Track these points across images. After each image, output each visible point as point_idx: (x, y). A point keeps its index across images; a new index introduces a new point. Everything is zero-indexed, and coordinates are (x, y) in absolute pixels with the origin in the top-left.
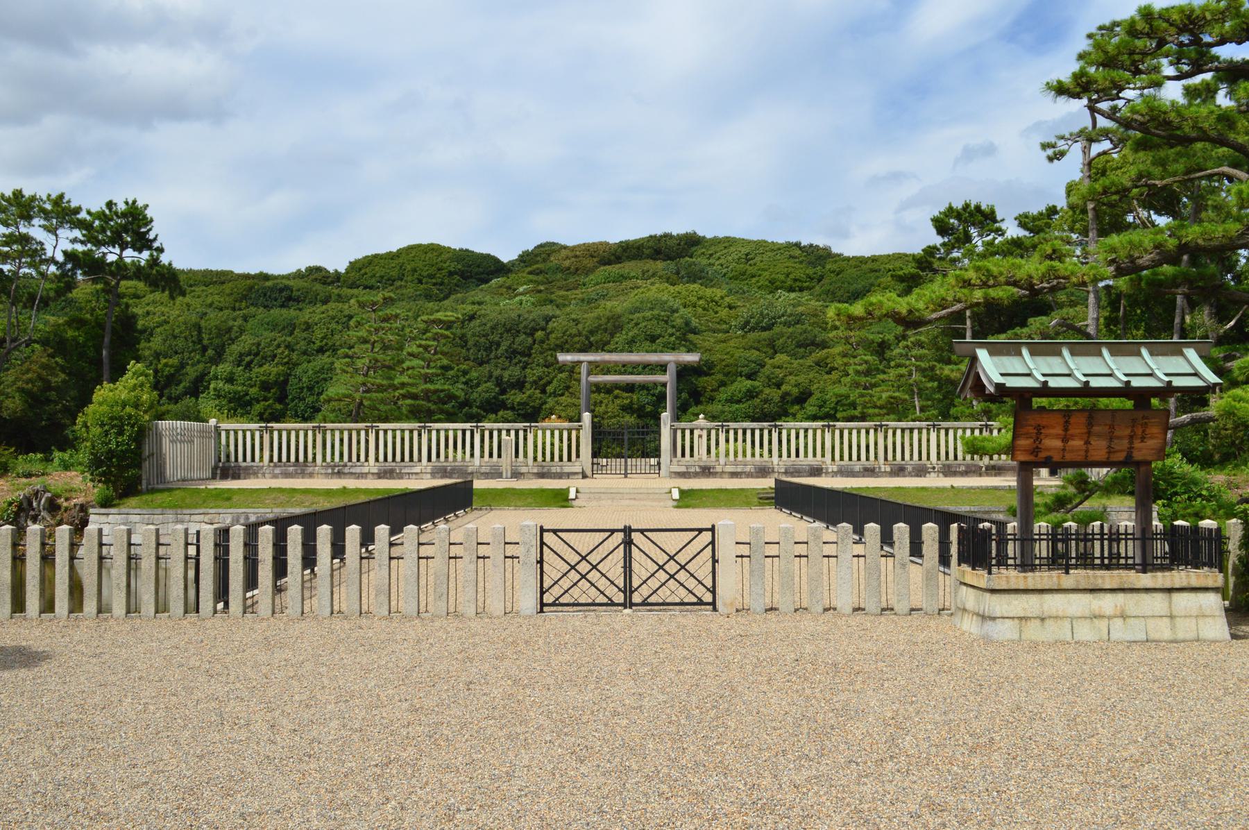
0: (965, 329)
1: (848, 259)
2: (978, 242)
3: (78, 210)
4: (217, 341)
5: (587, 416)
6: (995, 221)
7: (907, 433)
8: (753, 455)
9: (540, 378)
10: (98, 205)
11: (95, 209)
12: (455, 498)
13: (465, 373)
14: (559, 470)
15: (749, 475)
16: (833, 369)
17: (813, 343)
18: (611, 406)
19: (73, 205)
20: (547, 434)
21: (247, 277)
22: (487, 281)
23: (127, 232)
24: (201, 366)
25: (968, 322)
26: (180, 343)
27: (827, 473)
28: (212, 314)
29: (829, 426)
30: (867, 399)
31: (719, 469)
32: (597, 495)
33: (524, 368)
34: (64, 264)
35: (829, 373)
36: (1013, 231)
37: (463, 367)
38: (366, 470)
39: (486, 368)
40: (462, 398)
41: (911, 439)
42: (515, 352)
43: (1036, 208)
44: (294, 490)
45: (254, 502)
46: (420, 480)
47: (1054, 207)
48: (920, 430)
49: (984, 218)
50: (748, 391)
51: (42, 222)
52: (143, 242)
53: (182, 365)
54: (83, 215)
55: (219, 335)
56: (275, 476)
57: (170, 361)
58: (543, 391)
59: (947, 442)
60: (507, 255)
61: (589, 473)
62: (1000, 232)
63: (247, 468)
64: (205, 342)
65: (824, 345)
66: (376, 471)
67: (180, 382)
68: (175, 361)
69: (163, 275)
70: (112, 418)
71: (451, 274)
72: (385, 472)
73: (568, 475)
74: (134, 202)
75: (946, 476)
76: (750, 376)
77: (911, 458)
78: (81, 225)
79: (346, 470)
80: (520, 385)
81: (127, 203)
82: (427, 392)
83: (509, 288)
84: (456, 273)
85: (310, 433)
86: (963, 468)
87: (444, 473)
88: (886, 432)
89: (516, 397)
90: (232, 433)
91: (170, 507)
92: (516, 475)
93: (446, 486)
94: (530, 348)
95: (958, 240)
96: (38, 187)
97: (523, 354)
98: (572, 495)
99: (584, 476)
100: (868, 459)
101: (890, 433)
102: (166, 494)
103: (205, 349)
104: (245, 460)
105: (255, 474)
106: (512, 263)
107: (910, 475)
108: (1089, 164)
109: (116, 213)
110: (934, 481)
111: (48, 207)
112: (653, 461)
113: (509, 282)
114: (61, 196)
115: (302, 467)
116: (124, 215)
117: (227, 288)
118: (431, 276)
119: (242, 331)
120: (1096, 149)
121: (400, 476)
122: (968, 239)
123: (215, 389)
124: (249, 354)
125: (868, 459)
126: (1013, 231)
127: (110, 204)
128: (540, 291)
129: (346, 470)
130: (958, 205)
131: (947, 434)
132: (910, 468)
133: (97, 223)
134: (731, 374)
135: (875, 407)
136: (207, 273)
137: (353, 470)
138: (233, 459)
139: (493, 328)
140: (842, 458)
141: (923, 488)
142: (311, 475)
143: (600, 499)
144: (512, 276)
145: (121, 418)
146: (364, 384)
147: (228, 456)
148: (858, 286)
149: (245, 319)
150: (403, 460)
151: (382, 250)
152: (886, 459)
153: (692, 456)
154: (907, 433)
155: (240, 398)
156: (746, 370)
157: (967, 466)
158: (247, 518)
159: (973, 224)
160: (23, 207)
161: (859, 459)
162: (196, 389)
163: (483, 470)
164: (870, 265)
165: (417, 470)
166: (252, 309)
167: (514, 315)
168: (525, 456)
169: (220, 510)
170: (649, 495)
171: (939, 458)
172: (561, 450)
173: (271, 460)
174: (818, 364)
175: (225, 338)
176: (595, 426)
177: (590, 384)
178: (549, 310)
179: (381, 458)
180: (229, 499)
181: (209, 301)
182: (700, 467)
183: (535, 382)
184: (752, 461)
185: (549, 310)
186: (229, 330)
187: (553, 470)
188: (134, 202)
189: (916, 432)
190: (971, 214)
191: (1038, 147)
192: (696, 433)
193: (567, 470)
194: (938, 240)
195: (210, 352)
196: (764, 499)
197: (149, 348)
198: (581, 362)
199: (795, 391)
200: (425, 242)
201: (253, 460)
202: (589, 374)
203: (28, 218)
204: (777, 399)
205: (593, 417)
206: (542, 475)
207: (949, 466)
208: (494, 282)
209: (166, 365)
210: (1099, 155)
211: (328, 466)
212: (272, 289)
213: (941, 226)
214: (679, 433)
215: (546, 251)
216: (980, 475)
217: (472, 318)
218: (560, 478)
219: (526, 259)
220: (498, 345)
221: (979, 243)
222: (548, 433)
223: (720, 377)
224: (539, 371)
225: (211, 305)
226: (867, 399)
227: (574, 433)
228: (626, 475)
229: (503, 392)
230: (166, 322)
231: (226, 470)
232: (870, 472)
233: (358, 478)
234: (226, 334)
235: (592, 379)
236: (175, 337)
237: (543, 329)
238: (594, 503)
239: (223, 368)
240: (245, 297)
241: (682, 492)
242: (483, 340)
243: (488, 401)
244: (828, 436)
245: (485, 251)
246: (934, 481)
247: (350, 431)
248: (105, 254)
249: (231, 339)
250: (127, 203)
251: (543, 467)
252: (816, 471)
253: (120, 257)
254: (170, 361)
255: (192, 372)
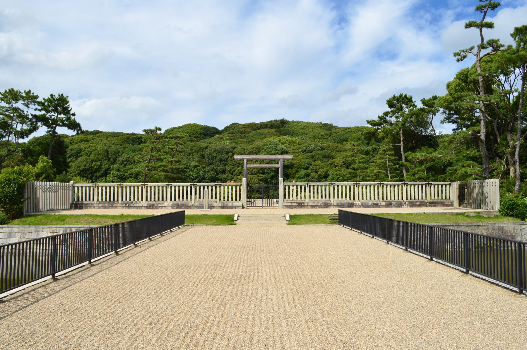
0: (400, 146)
1: (340, 128)
2: (406, 110)
3: (37, 97)
4: (114, 156)
5: (244, 180)
6: (412, 102)
7: (392, 187)
8: (314, 197)
9: (231, 170)
10: (47, 96)
11: (46, 98)
12: (175, 220)
13: (204, 168)
14: (231, 205)
15: (320, 207)
16: (337, 166)
17: (330, 157)
18: (255, 180)
19: (35, 94)
20: (225, 189)
21: (128, 134)
22: (213, 136)
23: (59, 106)
24: (107, 165)
25: (402, 143)
26: (100, 157)
27: (356, 206)
28: (113, 147)
29: (357, 184)
30: (365, 173)
31: (306, 204)
32: (249, 218)
33: (225, 166)
34: (32, 119)
35: (335, 167)
36: (420, 105)
37: (204, 166)
38: (141, 205)
39: (211, 166)
40: (202, 177)
41: (398, 189)
42: (222, 160)
43: (428, 97)
44: (97, 216)
45: (76, 222)
46: (166, 209)
47: (436, 96)
48: (398, 185)
49: (407, 100)
50: (306, 174)
51: (23, 102)
52: (66, 111)
53: (101, 165)
54: (39, 100)
55: (115, 154)
56: (99, 208)
57: (97, 164)
58: (232, 174)
59: (411, 190)
60: (221, 128)
61: (245, 206)
62: (415, 106)
63: (86, 204)
64: (110, 157)
65: (333, 157)
66: (146, 205)
67: (100, 171)
68: (98, 163)
69: (72, 124)
70: (5, 180)
71: (200, 134)
72: (150, 206)
73: (236, 207)
74: (62, 95)
75: (411, 207)
76: (307, 169)
77: (395, 199)
78: (39, 103)
79: (132, 205)
80: (224, 172)
81: (59, 95)
82: (172, 169)
83: (221, 138)
84: (202, 134)
85: (116, 188)
86: (418, 203)
87: (178, 206)
88: (383, 187)
89: (222, 176)
90: (80, 188)
91: (33, 224)
92: (211, 207)
93: (179, 212)
94: (227, 159)
95: (398, 109)
96: (21, 88)
97: (224, 161)
98: (236, 218)
99: (243, 208)
100: (375, 199)
101: (385, 187)
102: (33, 218)
103: (109, 159)
104: (86, 200)
105: (90, 207)
106: (223, 130)
107: (395, 206)
108: (480, 60)
109: (54, 99)
110: (405, 210)
111: (24, 95)
112: (275, 200)
113: (221, 137)
114: (30, 91)
115: (111, 203)
116: (57, 100)
117: (119, 138)
118: (193, 134)
119: (123, 153)
120: (483, 52)
121: (157, 208)
122: (402, 108)
123: (113, 174)
124: (126, 161)
125: (375, 199)
126: (420, 105)
127: (52, 95)
128: (232, 139)
129: (132, 205)
130: (397, 95)
131: (387, 187)
132: (394, 203)
133: (46, 103)
134: (300, 168)
135: (369, 177)
136: (114, 133)
137: (135, 205)
138: (80, 200)
139: (214, 152)
140: (363, 199)
141: (410, 214)
142: (116, 207)
143: (250, 220)
144: (222, 134)
145: (10, 180)
146: (147, 166)
147: (78, 197)
148: (344, 137)
149: (125, 148)
150: (159, 200)
151: (177, 126)
152: (359, 199)
153: (289, 198)
154: (392, 187)
155: (122, 177)
156: (305, 167)
157: (420, 202)
158: (71, 230)
159: (404, 103)
160: (13, 95)
161: (370, 199)
162: (106, 174)
163: (196, 205)
164: (348, 130)
165: (165, 205)
166: (127, 145)
167: (221, 147)
168: (216, 198)
169: (58, 226)
170: (274, 218)
171: (407, 199)
172: (232, 195)
173: (98, 200)
174: (331, 164)
175: (117, 155)
176: (248, 185)
177: (247, 168)
178: (234, 145)
179: (149, 199)
180: (64, 220)
181: (113, 142)
182: (297, 203)
183: (229, 171)
184: (322, 201)
185: (234, 145)
186: (119, 152)
187: (229, 205)
188: (62, 95)
189: (396, 187)
190: (403, 99)
191: (453, 55)
192: (291, 188)
193: (235, 205)
194: (389, 110)
195: (111, 160)
196: (333, 220)
197: (89, 159)
198: (243, 159)
199: (323, 174)
200: (192, 123)
201: (90, 200)
202: (247, 164)
203: (17, 100)
204: (316, 177)
205: (247, 180)
206: (223, 207)
207: (412, 202)
208: (216, 136)
209: (95, 165)
210: (485, 55)
211: (124, 203)
212: (135, 138)
213: (390, 104)
214: (287, 188)
215: (234, 126)
216: (426, 206)
217: (207, 148)
218: (232, 208)
219: (227, 129)
220: (216, 157)
221: (407, 110)
222: (226, 187)
223: (296, 169)
224: (230, 167)
225: (114, 143)
226: (365, 173)
227: (238, 188)
228: (262, 207)
229: (218, 174)
230: (96, 149)
231: (77, 205)
232: (376, 205)
233: (137, 209)
234: (117, 154)
235: (248, 166)
236: (99, 155)
237: (232, 152)
238: (247, 222)
239: (116, 166)
240: (126, 141)
241: (291, 216)
242: (210, 156)
243: (212, 178)
244: (356, 189)
245: (212, 126)
246: (405, 210)
247: (134, 187)
248: (51, 116)
249: (119, 155)
250: (59, 95)
251: (224, 203)
252: (351, 205)
253: (57, 117)
254: (97, 164)
255: (104, 167)
